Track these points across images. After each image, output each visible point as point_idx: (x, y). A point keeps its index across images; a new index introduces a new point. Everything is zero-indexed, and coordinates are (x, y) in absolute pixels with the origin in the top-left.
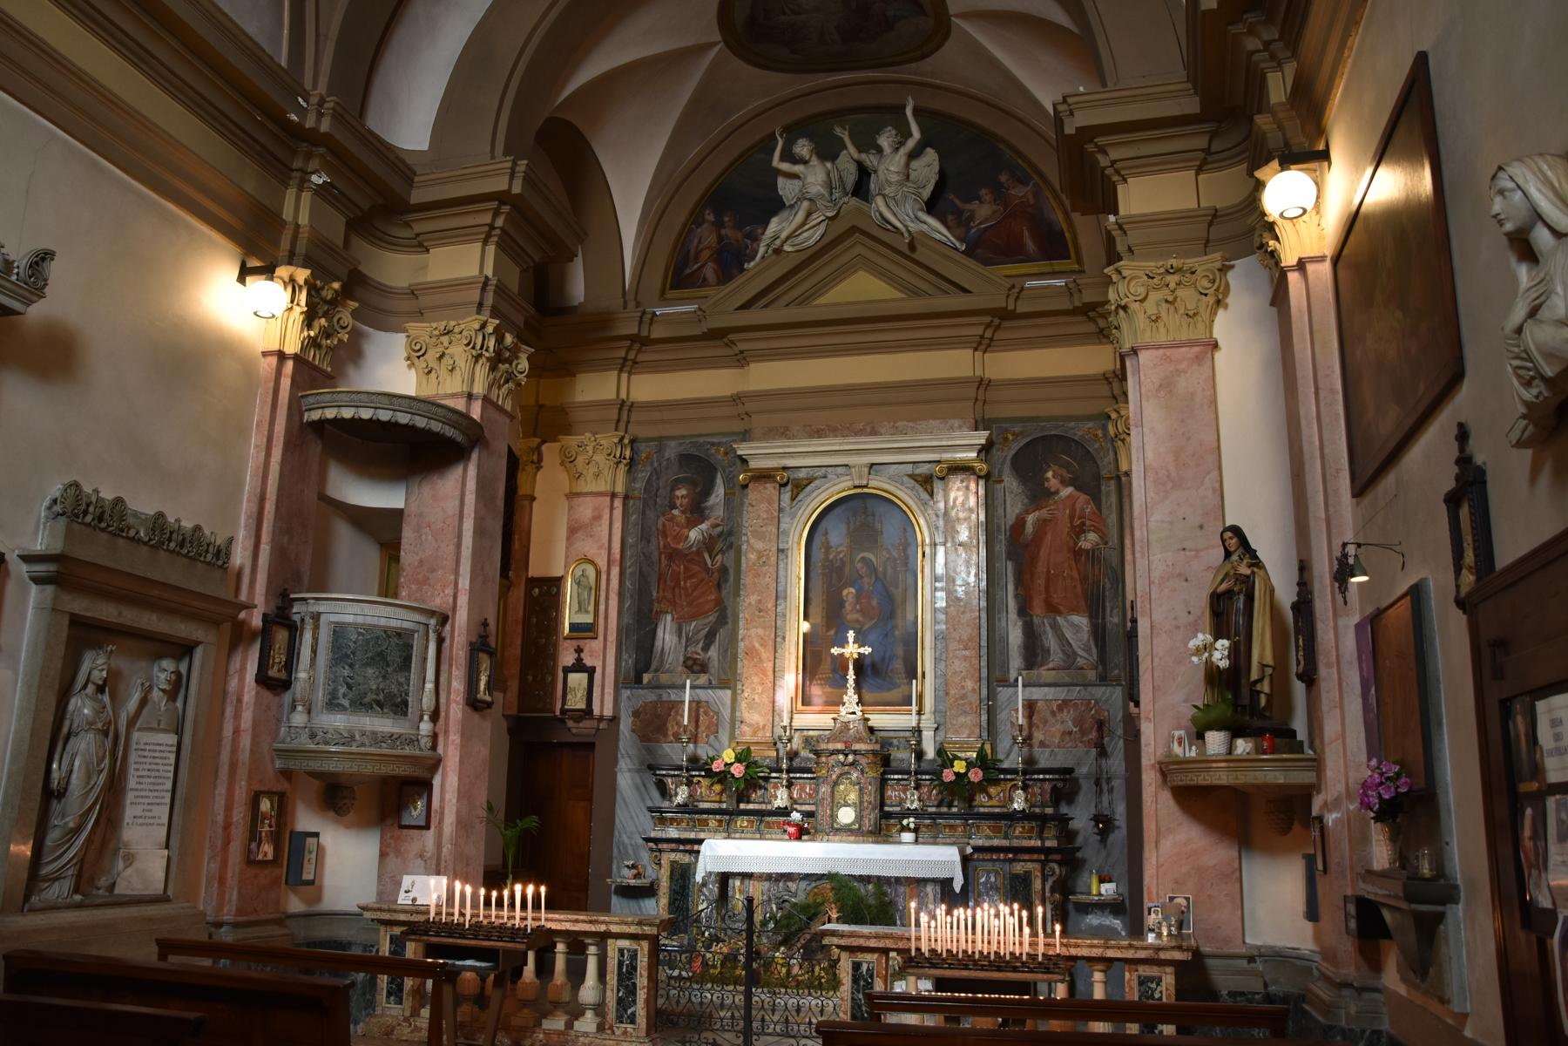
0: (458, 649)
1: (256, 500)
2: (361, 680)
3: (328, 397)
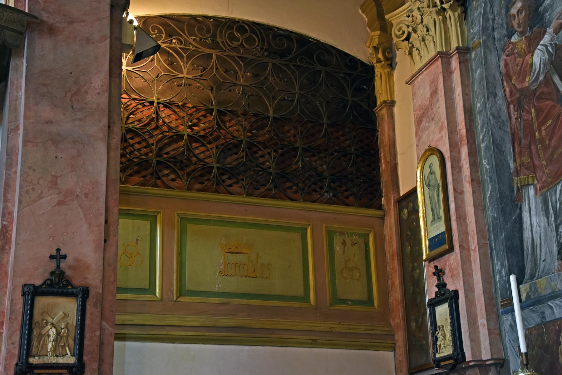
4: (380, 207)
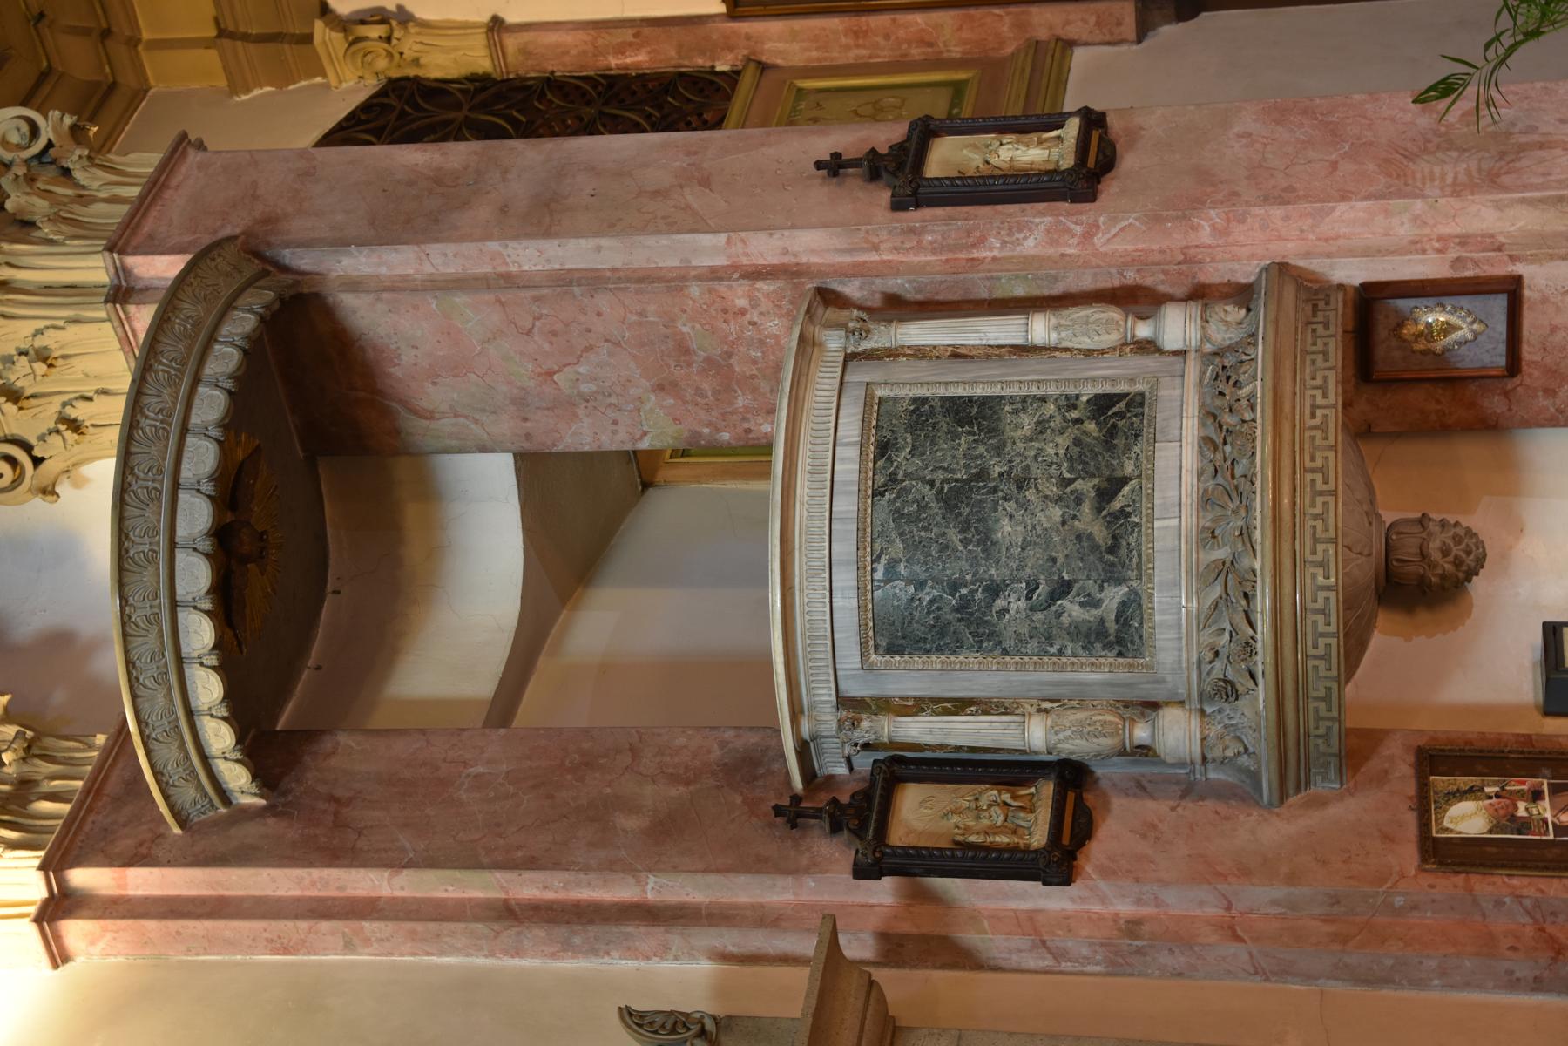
0: (919, 247)
1: (509, 935)
2: (1035, 556)
3: (168, 754)
4: (733, 76)
